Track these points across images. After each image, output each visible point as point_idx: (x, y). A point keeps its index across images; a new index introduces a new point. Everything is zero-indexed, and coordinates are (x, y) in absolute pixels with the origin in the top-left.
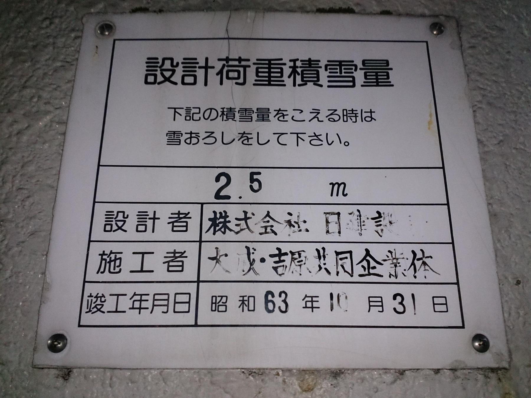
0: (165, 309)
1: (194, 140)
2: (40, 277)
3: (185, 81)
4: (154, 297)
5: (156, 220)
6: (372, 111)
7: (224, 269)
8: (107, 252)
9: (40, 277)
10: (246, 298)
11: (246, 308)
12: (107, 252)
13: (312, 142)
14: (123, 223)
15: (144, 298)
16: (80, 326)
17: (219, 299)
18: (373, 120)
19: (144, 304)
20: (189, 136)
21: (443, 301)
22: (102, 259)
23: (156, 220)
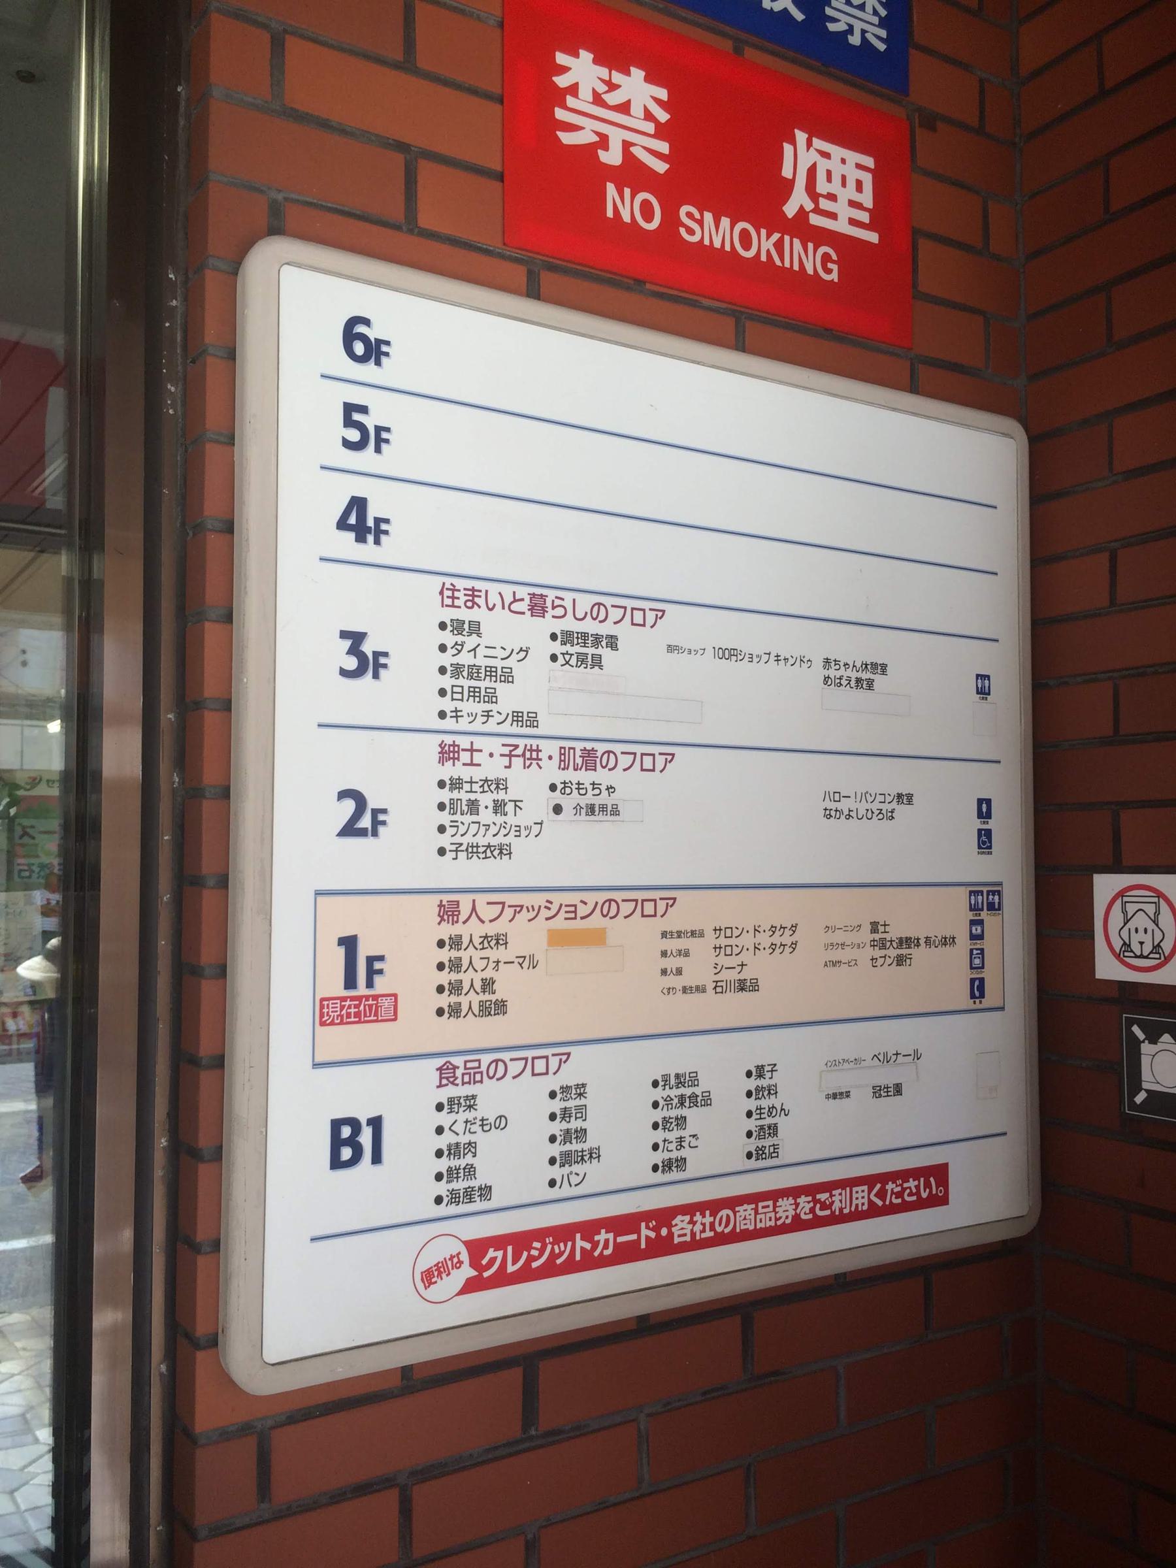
1: (568, 790)
2: (167, 492)
3: (461, 688)
5: (508, 758)
6: (458, 709)
7: (560, 787)
9: (167, 492)
13: (720, 650)
14: (523, 959)
16: (726, 937)
18: (475, 606)
20: (563, 785)
23: (508, 758)
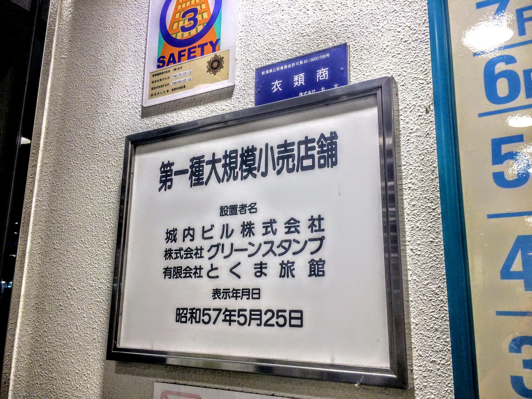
0: (247, 297)
4: (259, 296)
8: (286, 262)
10: (194, 311)
11: (194, 320)
12: (286, 262)
15: (232, 313)
17: (181, 311)
19: (238, 295)
21: (298, 315)
22: (282, 268)
